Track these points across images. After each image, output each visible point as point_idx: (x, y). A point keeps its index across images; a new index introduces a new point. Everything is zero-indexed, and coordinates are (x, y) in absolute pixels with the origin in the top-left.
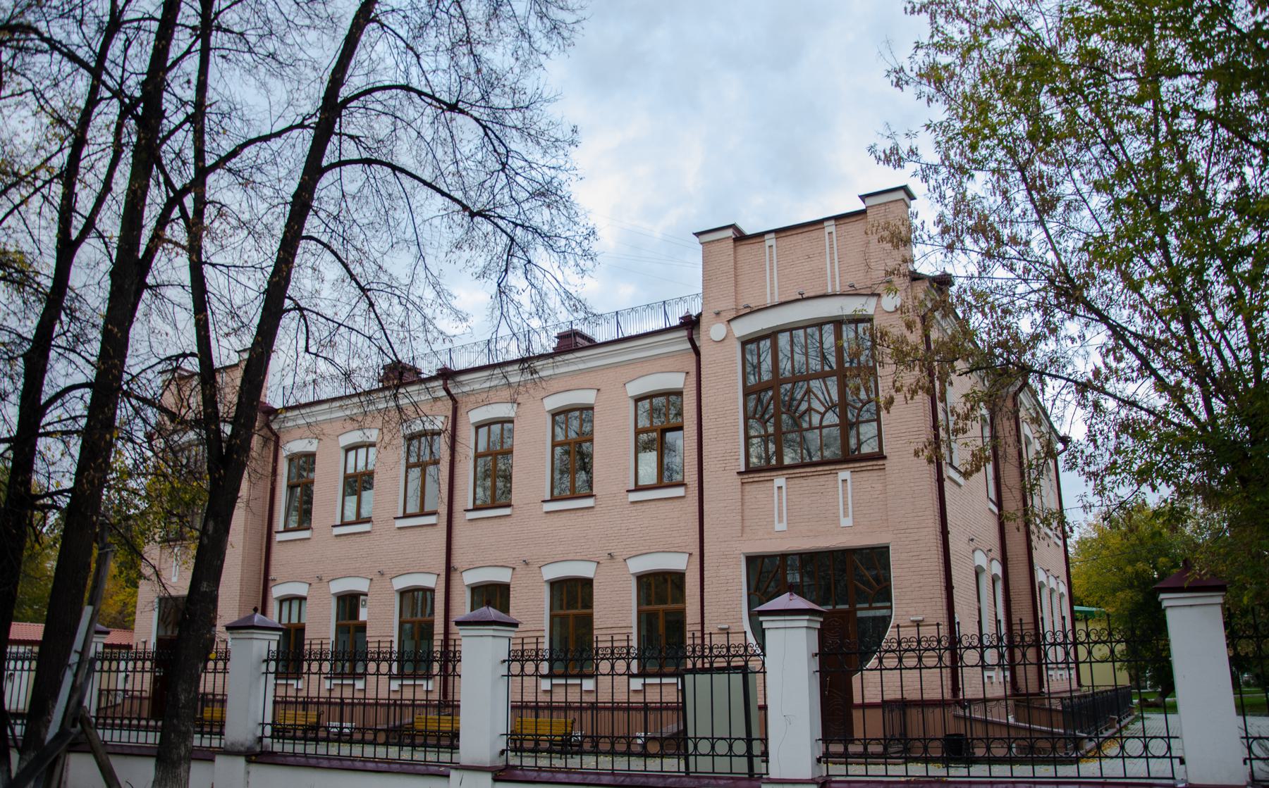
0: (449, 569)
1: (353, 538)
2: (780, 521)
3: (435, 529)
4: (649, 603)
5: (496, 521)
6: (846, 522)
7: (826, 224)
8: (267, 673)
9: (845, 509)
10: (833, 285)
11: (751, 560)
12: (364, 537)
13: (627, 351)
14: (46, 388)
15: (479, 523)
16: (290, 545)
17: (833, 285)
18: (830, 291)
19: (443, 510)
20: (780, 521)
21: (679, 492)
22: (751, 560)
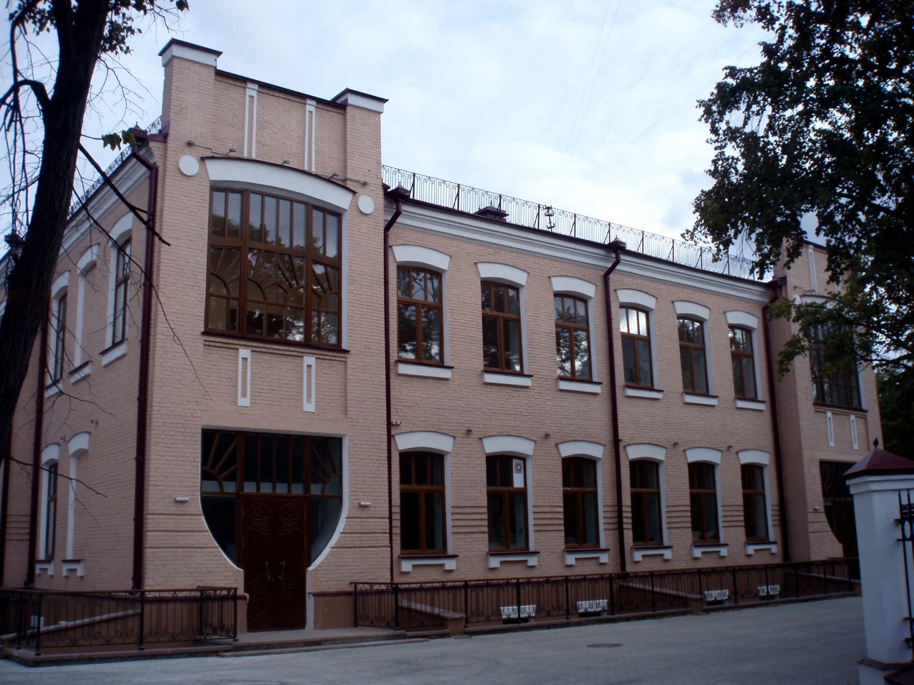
0: (616, 441)
1: (508, 390)
2: (309, 401)
3: (597, 398)
4: (583, 494)
5: (649, 402)
6: (309, 407)
7: (249, 85)
8: (904, 539)
9: (309, 395)
10: (250, 151)
11: (337, 441)
12: (521, 392)
13: (451, 225)
14: (77, 184)
15: (636, 402)
16: (419, 384)
17: (250, 151)
18: (246, 155)
19: (605, 380)
20: (244, 395)
21: (596, 389)
22: (337, 441)
